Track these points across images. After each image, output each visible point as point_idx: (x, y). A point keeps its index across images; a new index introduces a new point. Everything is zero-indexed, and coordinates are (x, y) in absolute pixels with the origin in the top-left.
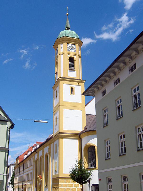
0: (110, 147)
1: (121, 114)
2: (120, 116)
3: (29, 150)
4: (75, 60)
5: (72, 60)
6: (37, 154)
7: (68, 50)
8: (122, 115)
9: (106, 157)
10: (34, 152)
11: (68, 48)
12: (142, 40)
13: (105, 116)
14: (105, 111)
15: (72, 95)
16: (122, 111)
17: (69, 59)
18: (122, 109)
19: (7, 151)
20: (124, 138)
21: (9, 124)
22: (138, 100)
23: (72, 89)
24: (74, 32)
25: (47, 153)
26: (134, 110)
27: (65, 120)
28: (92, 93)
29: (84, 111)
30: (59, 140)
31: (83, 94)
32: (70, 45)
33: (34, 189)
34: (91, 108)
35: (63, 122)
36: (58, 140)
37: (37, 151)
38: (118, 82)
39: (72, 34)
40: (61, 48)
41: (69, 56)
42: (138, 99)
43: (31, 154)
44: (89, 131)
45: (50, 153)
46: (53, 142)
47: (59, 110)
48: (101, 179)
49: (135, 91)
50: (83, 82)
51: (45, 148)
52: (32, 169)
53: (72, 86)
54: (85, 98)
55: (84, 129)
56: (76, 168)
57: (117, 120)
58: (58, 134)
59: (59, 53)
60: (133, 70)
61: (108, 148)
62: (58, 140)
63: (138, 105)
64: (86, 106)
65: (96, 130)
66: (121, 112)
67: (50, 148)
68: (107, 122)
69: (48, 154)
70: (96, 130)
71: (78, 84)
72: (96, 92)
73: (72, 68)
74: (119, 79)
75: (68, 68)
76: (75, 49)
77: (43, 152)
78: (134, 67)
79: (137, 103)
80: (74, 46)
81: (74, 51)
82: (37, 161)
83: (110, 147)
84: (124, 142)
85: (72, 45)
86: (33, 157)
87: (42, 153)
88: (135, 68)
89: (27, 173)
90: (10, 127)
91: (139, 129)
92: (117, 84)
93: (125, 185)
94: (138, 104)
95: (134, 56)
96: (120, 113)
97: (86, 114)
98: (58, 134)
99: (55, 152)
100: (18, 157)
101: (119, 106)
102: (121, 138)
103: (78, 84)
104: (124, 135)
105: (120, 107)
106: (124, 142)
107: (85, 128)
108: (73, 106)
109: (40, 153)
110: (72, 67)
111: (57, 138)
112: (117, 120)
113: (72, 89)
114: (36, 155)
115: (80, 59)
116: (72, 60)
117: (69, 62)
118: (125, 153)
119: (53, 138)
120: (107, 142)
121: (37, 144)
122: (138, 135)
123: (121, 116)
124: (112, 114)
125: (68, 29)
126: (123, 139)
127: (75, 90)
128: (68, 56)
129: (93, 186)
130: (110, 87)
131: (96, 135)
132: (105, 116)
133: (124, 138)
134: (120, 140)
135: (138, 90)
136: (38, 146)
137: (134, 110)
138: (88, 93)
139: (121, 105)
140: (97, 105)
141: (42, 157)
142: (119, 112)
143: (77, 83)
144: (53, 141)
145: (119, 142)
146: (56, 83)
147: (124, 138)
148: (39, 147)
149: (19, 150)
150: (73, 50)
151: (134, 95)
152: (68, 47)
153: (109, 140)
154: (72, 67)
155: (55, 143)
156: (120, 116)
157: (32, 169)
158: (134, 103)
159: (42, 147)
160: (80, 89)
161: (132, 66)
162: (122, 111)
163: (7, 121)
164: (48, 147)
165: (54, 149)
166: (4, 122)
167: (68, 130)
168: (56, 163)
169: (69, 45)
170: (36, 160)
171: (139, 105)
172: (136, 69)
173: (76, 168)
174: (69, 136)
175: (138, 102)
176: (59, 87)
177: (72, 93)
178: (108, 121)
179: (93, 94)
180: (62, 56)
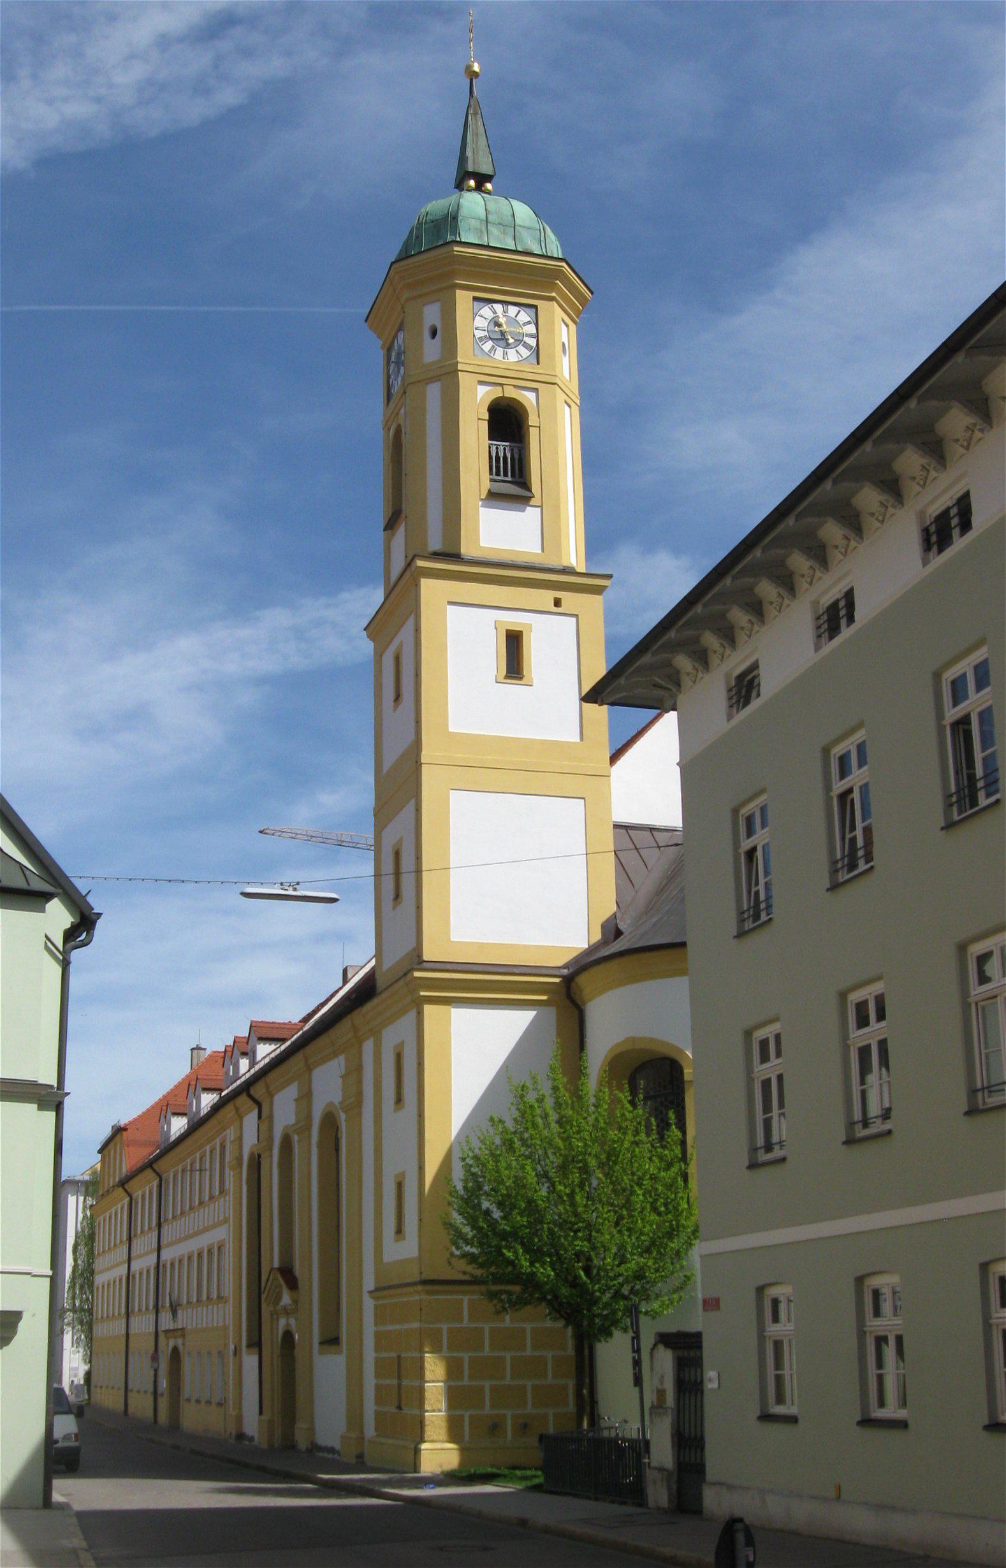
0: (780, 1078)
1: (861, 853)
2: (852, 859)
3: (193, 1085)
4: (532, 420)
5: (507, 421)
6: (256, 1111)
8: (869, 857)
9: (756, 1149)
12: (1005, 349)
13: (751, 853)
14: (749, 821)
15: (513, 689)
16: (867, 831)
17: (487, 416)
18: (866, 815)
19: (50, 1098)
20: (881, 1016)
21: (57, 917)
22: (978, 756)
23: (514, 641)
24: (523, 212)
25: (331, 1104)
26: (949, 826)
27: (457, 881)
28: (656, 686)
29: (595, 801)
31: (593, 696)
34: (651, 780)
36: (412, 1014)
37: (258, 1091)
38: (843, 622)
39: (512, 226)
40: (427, 333)
42: (983, 750)
43: (216, 1108)
44: (626, 950)
45: (354, 1104)
46: (376, 1033)
48: (717, 1301)
49: (958, 691)
51: (318, 1074)
52: (226, 1220)
53: (515, 620)
54: (610, 713)
55: (597, 936)
57: (834, 887)
58: (417, 974)
60: (951, 537)
61: (766, 1084)
62: (412, 1014)
63: (981, 795)
64: (614, 758)
65: (683, 945)
66: (859, 833)
67: (354, 1072)
68: (763, 906)
69: (343, 1116)
70: (683, 945)
71: (557, 603)
72: (686, 681)
74: (849, 595)
76: (532, 342)
77: (306, 1097)
78: (955, 522)
79: (972, 778)
80: (524, 317)
82: (256, 1163)
83: (780, 1078)
84: (883, 1044)
86: (231, 1134)
87: (293, 1105)
88: (966, 526)
90: (70, 935)
91: (983, 959)
92: (833, 630)
93: (881, 1340)
94: (980, 784)
95: (958, 440)
96: (853, 840)
97: (617, 826)
98: (417, 974)
100: (118, 1131)
101: (850, 791)
102: (863, 1022)
103: (557, 603)
104: (880, 1001)
105: (856, 795)
106: (883, 1044)
107: (612, 930)
108: (518, 768)
109: (284, 1107)
110: (506, 474)
112: (834, 887)
113: (514, 641)
114: (251, 1120)
116: (507, 421)
117: (487, 442)
118: (888, 1126)
119: (384, 995)
120: (764, 1044)
121: (254, 1038)
122: (976, 1004)
123: (861, 862)
124: (797, 844)
125: (479, 188)
126: (875, 1031)
127: (534, 653)
128: (482, 390)
129: (661, 1347)
130: (783, 648)
131: (685, 980)
132: (751, 853)
133: (866, 763)
134: (852, 1036)
135: (980, 687)
136: (265, 1051)
137: (949, 826)
138: (632, 683)
139: (865, 789)
140: (695, 772)
141: (296, 1138)
142: (848, 836)
143: (549, 596)
145: (846, 1048)
147: (881, 1016)
148: (276, 1063)
149: (128, 1077)
150: (521, 348)
151: (955, 718)
152: (479, 322)
153: (775, 1028)
154: (506, 474)
155: (392, 1036)
156: (852, 859)
157: (226, 1220)
158: (957, 773)
159: (297, 1061)
160: (565, 649)
161: (943, 508)
162: (867, 831)
163: (47, 897)
165: (384, 1082)
166: (29, 898)
167: (481, 946)
169: (486, 311)
170: (252, 1155)
171: (988, 795)
172: (971, 536)
174: (486, 983)
175: (979, 772)
176: (417, 630)
178: (768, 898)
179: (660, 692)
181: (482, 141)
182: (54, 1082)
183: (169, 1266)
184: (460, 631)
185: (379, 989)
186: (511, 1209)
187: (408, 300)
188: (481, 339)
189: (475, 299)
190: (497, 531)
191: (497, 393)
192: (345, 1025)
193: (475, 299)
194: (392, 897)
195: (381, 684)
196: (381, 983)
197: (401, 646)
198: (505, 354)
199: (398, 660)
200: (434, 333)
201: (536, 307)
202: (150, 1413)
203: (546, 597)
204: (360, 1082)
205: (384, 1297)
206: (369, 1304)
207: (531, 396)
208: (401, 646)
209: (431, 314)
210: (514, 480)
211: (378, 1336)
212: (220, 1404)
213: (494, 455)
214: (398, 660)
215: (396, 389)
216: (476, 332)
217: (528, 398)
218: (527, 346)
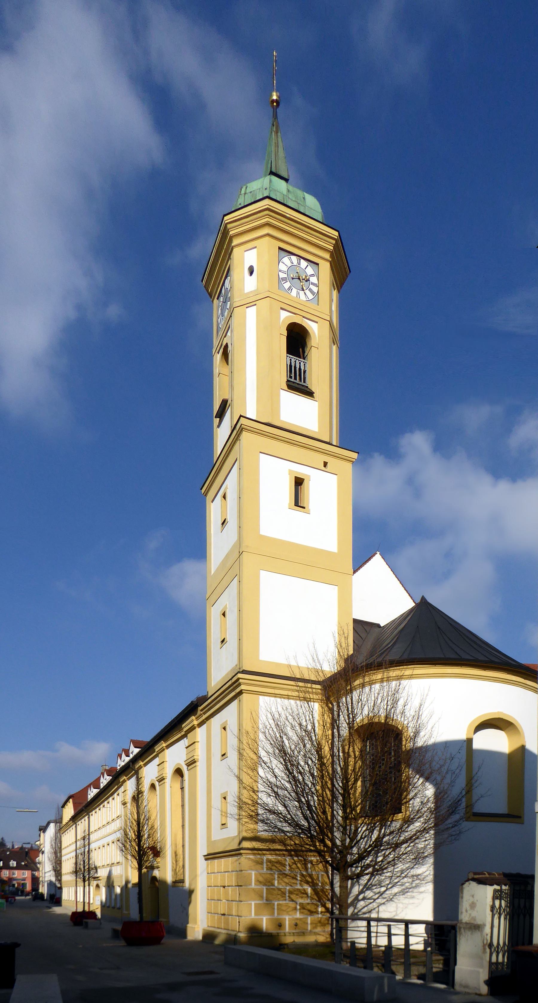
5: (297, 340)
7: (280, 287)
11: (282, 275)
15: (298, 514)
17: (285, 333)
23: (299, 482)
25: (179, 764)
32: (294, 258)
35: (227, 674)
41: (286, 317)
47: (238, 576)
53: (302, 471)
56: (378, 732)
59: (237, 299)
64: (355, 572)
71: (325, 464)
73: (298, 385)
75: (281, 376)
76: (315, 289)
81: (311, 296)
85: (304, 264)
89: (100, 843)
103: (325, 464)
108: (300, 561)
110: (295, 379)
113: (299, 482)
115: (334, 348)
128: (284, 315)
154: (295, 379)
169: (286, 260)
173: (378, 732)
177: (298, 503)
180: (251, 313)
182: (424, 926)
183: (238, 690)
186: (258, 804)
194: (221, 523)
197: (226, 488)
198: (298, 294)
200: (251, 272)
201: (317, 264)
212: (119, 909)
213: (289, 364)
216: (280, 273)
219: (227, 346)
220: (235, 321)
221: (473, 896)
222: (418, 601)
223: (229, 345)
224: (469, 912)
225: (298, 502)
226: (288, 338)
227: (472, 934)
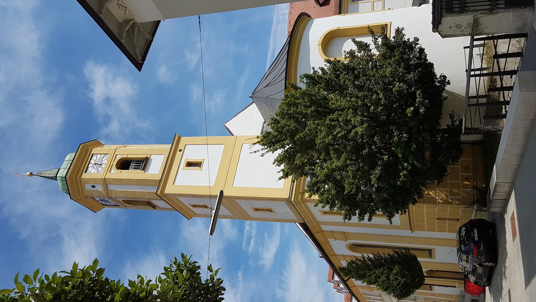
4: (125, 156)
5: (124, 164)
10: (350, 285)
15: (204, 165)
23: (190, 164)
30: (477, 94)
32: (90, 166)
33: (492, 301)
40: (94, 189)
50: (179, 138)
53: (183, 163)
58: (293, 200)
64: (232, 135)
71: (180, 150)
73: (142, 163)
85: (92, 161)
98: (293, 200)
99: (258, 206)
103: (180, 150)
111: (302, 204)
113: (190, 164)
116: (124, 164)
119: (306, 222)
128: (112, 171)
144: (316, 225)
146: (299, 211)
164: (332, 241)
168: (270, 211)
169: (89, 169)
181: (49, 172)
184: (184, 181)
185: (303, 222)
187: (83, 195)
188: (97, 171)
189: (85, 172)
190: (155, 169)
191: (114, 166)
192: (317, 236)
193: (85, 172)
194: (270, 213)
195: (205, 215)
196: (302, 222)
197: (189, 204)
199: (194, 206)
200: (94, 187)
202: (486, 78)
203: (179, 154)
204: (336, 232)
205: (414, 227)
206: (417, 234)
207: (118, 156)
208: (189, 204)
209: (88, 187)
210: (142, 163)
211: (429, 230)
214: (194, 206)
215: (113, 203)
217: (119, 157)
218: (103, 158)
219: (123, 201)
220: (113, 196)
221: (451, 27)
222: (251, 100)
223: (123, 199)
224: (463, 29)
225: (198, 164)
226: (122, 169)
227: (481, 25)
